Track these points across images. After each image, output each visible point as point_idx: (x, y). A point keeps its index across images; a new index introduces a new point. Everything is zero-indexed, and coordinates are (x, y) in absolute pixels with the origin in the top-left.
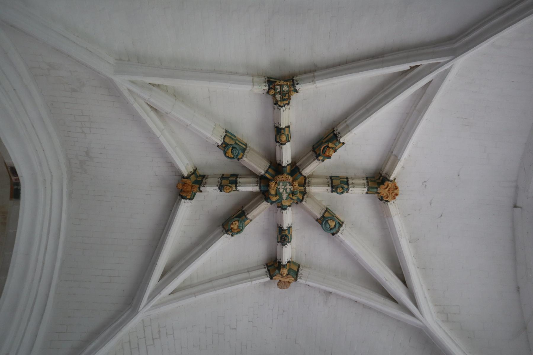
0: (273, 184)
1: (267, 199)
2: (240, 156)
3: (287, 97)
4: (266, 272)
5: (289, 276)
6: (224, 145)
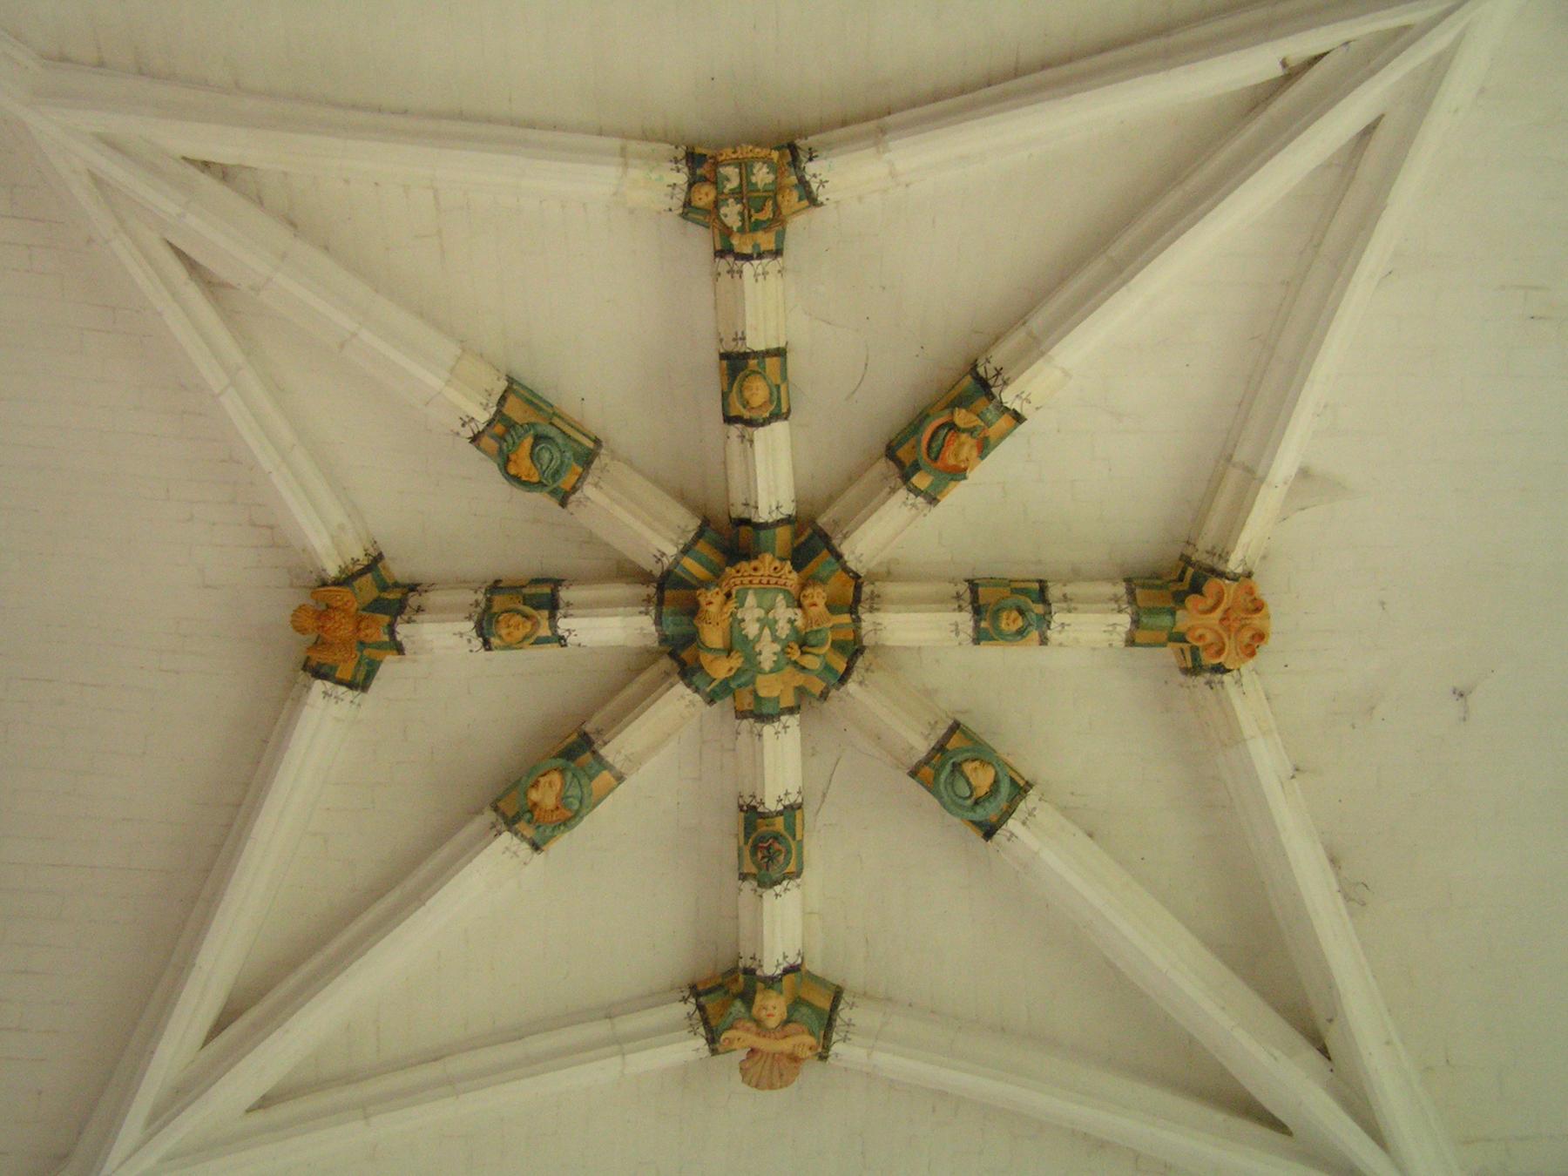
0: (712, 601)
1: (689, 672)
2: (567, 481)
3: (767, 214)
4: (690, 1016)
5: (791, 1027)
6: (499, 429)
